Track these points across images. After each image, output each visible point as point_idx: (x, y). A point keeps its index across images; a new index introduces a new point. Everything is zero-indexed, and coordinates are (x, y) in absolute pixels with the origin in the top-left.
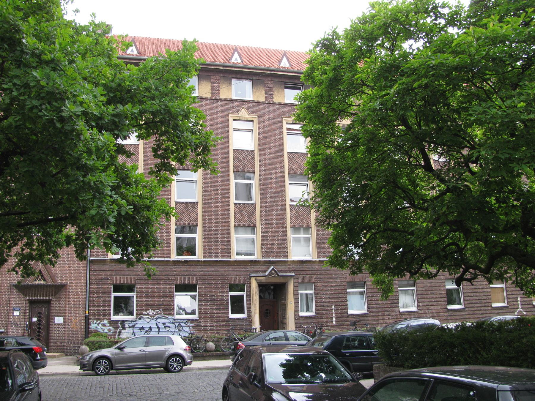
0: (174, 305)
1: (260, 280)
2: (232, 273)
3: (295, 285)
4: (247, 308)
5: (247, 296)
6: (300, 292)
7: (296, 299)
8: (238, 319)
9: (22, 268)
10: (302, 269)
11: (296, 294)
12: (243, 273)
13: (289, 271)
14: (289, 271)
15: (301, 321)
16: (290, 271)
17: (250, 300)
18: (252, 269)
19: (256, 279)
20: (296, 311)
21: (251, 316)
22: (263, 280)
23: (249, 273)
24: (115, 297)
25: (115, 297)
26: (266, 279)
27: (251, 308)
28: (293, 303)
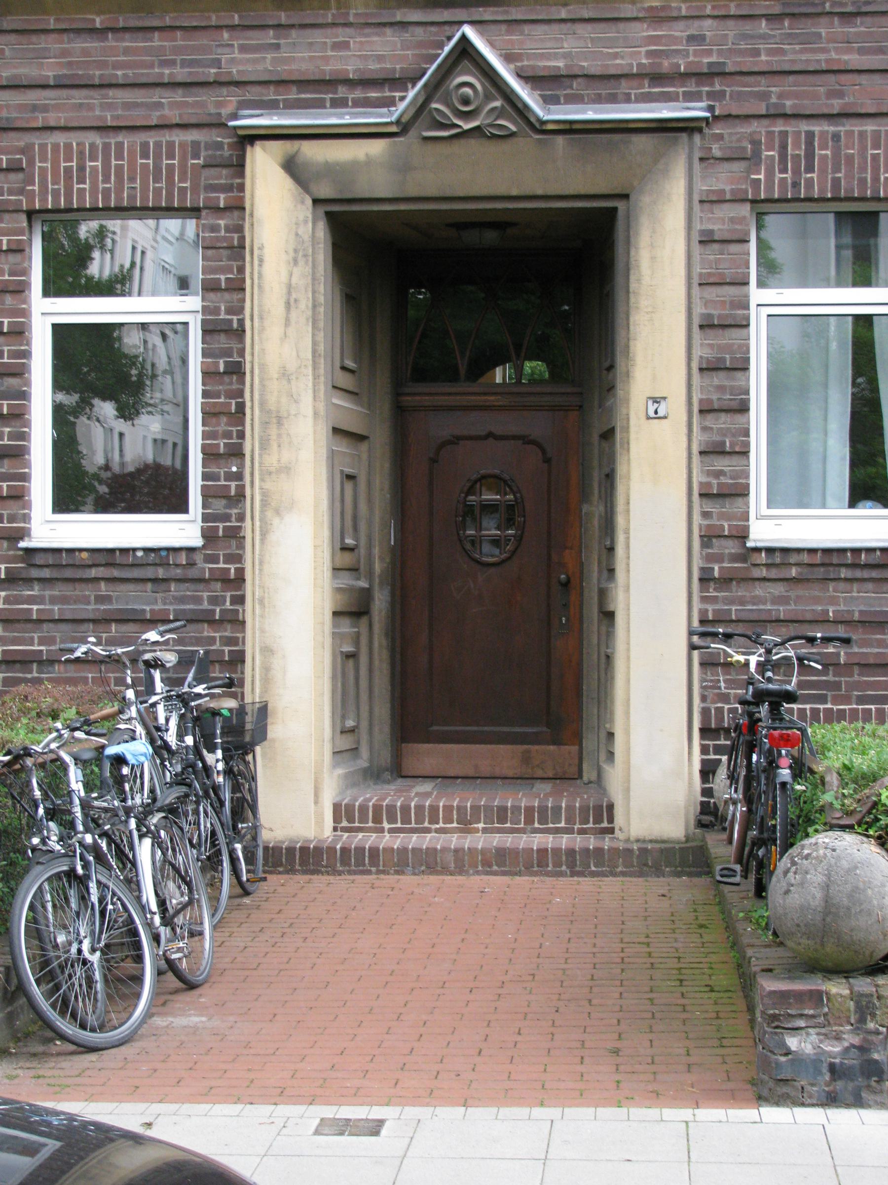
0: (206, 518)
1: (330, 170)
2: (61, 107)
3: (720, 220)
4: (210, 455)
5: (208, 331)
6: (766, 301)
7: (719, 370)
8: (108, 557)
9: (98, 953)
10: (795, 56)
11: (719, 326)
12: (170, 105)
13: (657, 78)
14: (657, 78)
15: (765, 599)
16: (657, 79)
17: (236, 370)
18: (263, 65)
19: (290, 166)
20: (720, 495)
21: (235, 535)
22: (368, 165)
23: (209, 103)
24: (61, 332)
25: (61, 332)
26: (402, 167)
27: (236, 453)
28: (676, 407)
